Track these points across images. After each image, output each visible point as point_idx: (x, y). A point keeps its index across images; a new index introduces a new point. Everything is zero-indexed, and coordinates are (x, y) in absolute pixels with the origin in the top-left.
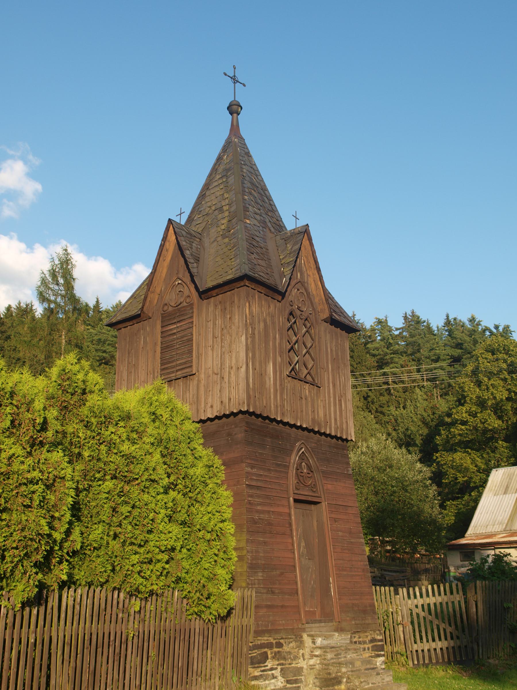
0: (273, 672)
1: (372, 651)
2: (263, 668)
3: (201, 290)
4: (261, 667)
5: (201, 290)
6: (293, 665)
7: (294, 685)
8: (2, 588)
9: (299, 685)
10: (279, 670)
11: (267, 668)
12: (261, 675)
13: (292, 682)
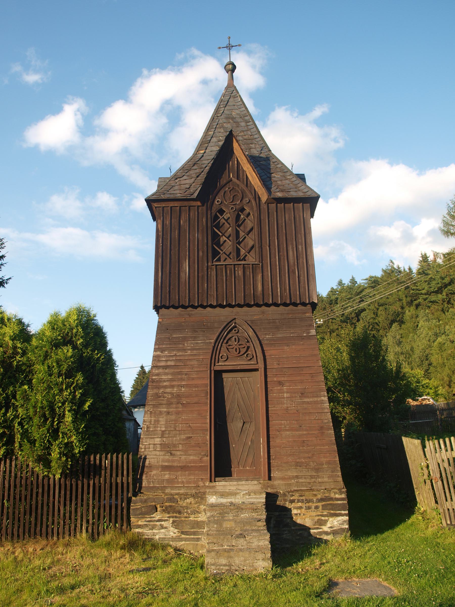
0: (162, 523)
1: (323, 509)
2: (149, 519)
3: (309, 204)
4: (147, 518)
5: (309, 204)
6: (191, 519)
7: (192, 537)
8: (454, 356)
9: (200, 536)
10: (171, 522)
11: (154, 519)
12: (146, 524)
13: (189, 533)
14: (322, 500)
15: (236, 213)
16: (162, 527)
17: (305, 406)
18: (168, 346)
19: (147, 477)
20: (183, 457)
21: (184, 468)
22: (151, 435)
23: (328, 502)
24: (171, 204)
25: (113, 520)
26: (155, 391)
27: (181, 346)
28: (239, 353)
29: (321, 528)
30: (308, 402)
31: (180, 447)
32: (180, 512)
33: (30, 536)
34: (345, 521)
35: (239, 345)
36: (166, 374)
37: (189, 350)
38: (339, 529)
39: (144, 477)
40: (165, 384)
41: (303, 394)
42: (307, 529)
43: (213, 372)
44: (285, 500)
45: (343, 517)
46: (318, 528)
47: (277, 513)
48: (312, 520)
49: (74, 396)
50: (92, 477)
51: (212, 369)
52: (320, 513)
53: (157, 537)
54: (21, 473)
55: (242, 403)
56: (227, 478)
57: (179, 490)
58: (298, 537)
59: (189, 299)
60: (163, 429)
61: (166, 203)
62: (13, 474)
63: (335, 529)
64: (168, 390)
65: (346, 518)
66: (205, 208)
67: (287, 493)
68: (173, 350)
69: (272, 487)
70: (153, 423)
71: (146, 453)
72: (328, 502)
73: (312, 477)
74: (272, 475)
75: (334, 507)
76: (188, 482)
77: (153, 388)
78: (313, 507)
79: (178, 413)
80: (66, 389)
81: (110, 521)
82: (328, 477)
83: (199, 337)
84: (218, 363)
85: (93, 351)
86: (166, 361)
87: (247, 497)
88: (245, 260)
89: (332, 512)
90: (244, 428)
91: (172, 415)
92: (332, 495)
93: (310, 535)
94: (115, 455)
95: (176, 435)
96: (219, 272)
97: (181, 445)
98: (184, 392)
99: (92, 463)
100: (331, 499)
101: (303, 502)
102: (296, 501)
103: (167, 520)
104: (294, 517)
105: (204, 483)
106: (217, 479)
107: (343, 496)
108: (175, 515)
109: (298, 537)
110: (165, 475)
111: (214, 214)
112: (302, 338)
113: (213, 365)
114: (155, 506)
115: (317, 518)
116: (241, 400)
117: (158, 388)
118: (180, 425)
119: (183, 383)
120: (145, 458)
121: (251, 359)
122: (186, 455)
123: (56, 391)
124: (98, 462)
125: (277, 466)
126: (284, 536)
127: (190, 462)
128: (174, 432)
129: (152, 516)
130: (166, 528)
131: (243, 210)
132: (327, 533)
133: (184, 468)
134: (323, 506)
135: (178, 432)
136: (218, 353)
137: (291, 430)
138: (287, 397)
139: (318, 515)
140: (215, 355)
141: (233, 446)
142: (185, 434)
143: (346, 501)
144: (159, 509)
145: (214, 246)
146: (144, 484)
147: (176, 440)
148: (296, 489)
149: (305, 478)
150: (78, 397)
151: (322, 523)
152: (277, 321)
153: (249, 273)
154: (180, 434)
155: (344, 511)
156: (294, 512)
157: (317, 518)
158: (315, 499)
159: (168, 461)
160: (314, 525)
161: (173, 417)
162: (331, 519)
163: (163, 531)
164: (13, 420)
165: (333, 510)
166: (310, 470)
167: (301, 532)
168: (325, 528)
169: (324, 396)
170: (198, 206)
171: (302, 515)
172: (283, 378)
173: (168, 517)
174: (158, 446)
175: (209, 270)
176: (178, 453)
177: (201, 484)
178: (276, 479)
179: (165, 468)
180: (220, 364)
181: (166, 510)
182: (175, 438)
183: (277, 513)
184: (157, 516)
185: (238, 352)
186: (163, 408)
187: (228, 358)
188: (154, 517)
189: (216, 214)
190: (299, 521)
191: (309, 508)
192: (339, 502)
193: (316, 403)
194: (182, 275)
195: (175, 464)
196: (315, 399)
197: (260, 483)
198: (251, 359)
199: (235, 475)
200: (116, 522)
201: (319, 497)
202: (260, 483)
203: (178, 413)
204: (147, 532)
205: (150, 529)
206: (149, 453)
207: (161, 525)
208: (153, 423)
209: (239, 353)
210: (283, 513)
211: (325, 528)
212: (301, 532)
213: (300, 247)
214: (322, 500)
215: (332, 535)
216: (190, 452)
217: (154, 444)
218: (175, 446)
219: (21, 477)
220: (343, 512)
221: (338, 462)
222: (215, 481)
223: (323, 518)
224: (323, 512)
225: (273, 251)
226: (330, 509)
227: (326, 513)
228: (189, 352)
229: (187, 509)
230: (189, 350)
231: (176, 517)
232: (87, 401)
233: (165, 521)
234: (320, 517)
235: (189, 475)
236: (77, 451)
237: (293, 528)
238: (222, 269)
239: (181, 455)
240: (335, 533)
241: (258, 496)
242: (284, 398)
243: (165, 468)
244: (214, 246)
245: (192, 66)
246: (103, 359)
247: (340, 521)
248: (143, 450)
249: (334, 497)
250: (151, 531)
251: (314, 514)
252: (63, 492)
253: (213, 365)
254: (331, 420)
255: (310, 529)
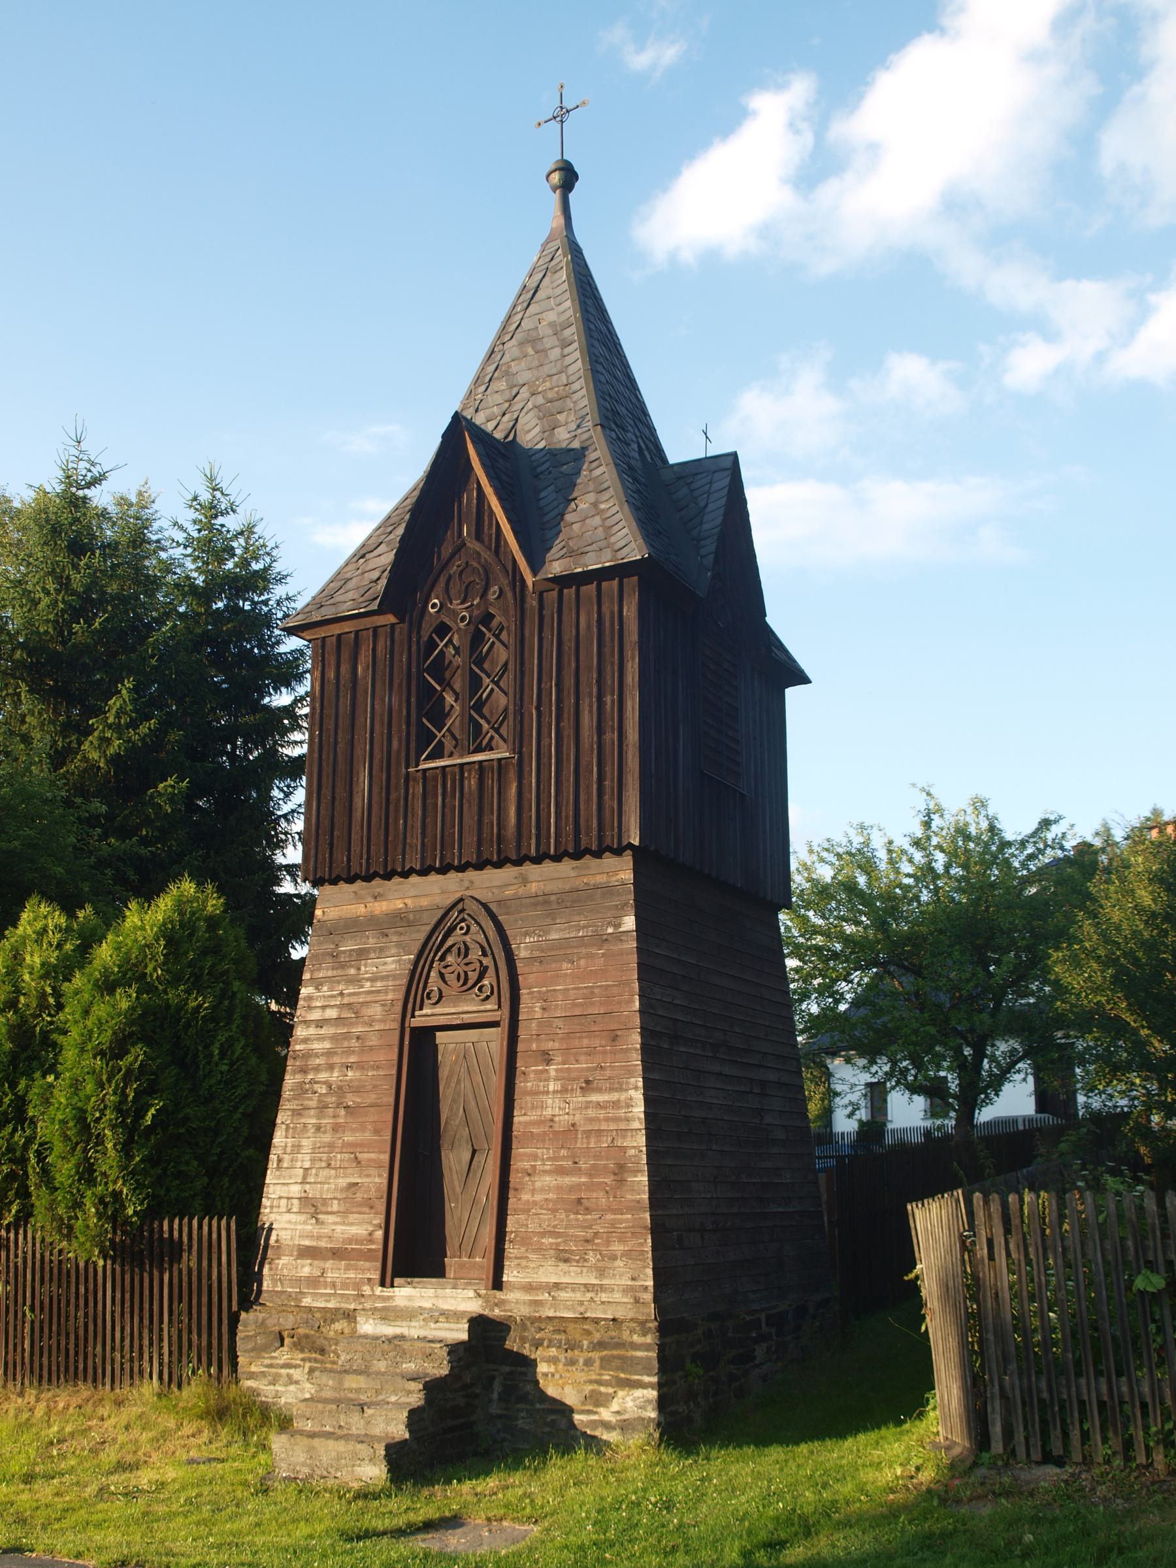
0: (292, 1371)
1: (602, 1367)
10: (307, 1370)
14: (601, 1345)
15: (472, 628)
16: (291, 1381)
17: (591, 1113)
18: (330, 973)
19: (271, 1269)
20: (339, 1228)
21: (336, 1254)
22: (284, 1178)
23: (615, 1352)
24: (336, 629)
25: (204, 1359)
26: (299, 1078)
27: (352, 971)
28: (465, 983)
29: (596, 1413)
30: (598, 1103)
31: (335, 1206)
32: (322, 1351)
33: (67, 1381)
34: (648, 1401)
35: (467, 964)
36: (321, 1038)
37: (367, 980)
38: (635, 1419)
39: (266, 1271)
40: (318, 1061)
41: (588, 1086)
42: (566, 1411)
43: (408, 1031)
44: (523, 1340)
45: (645, 1391)
46: (589, 1412)
47: (507, 1369)
48: (579, 1392)
49: (124, 1095)
50: (166, 1265)
51: (407, 1025)
52: (594, 1377)
53: (283, 1400)
54: (51, 1254)
55: (473, 1103)
56: (416, 1280)
57: (327, 1301)
58: (547, 1429)
59: (368, 859)
60: (307, 1165)
61: (324, 628)
62: (38, 1256)
63: (626, 1417)
64: (323, 1076)
65: (653, 1394)
66: (405, 626)
67: (528, 1323)
68: (339, 982)
69: (500, 1304)
70: (289, 1150)
71: (273, 1217)
72: (615, 1352)
73: (587, 1287)
74: (505, 1278)
75: (627, 1364)
76: (345, 1286)
77: (294, 1073)
78: (581, 1361)
79: (336, 1128)
80: (109, 1081)
81: (199, 1360)
82: (624, 1291)
83: (388, 947)
84: (421, 1009)
85: (188, 992)
86: (324, 1007)
87: (433, 1325)
88: (491, 749)
89: (622, 1375)
90: (474, 1162)
91: (325, 1132)
92: (625, 1335)
93: (572, 1425)
94: (177, 1221)
95: (330, 1178)
96: (429, 788)
97: (336, 1202)
98: (351, 1081)
99: (166, 1236)
100: (621, 1345)
101: (559, 1347)
102: (545, 1344)
103: (299, 1366)
104: (541, 1381)
105: (372, 1290)
106: (397, 1281)
107: (649, 1339)
108: (314, 1355)
109: (547, 1429)
110: (303, 1266)
111: (426, 639)
112: (603, 940)
113: (409, 1015)
114: (280, 1333)
115: (589, 1387)
116: (471, 1096)
117: (304, 1071)
118: (339, 1156)
119: (352, 1059)
120: (270, 1229)
121: (488, 998)
122: (343, 1224)
123: (90, 1087)
124: (176, 1234)
125: (516, 1258)
126: (520, 1422)
127: (350, 1241)
128: (326, 1172)
129: (273, 1354)
130: (297, 1382)
131: (487, 618)
132: (607, 1426)
133: (336, 1254)
134: (602, 1359)
135: (333, 1172)
136: (421, 986)
137: (560, 1171)
138: (554, 1092)
139: (591, 1382)
140: (415, 990)
141: (450, 1206)
142: (345, 1176)
143: (653, 1350)
144: (287, 1341)
145: (424, 720)
146: (265, 1287)
147: (328, 1190)
148: (551, 1315)
149: (573, 1290)
150: (131, 1098)
151: (599, 1400)
152: (553, 898)
153: (491, 783)
154: (336, 1177)
155: (648, 1375)
156: (542, 1368)
157: (589, 1387)
158: (585, 1343)
159: (311, 1237)
160: (583, 1404)
161: (327, 1138)
162: (621, 1393)
163: (292, 1388)
164: (26, 1147)
165: (623, 1371)
166: (585, 1270)
167: (554, 1417)
168: (606, 1414)
169: (636, 1088)
170: (393, 625)
171: (557, 1376)
172: (551, 1043)
173: (303, 1360)
174: (296, 1202)
175: (411, 783)
176: (330, 1219)
177: (367, 1290)
178: (513, 1287)
179: (307, 1253)
180: (424, 1012)
181: (298, 1346)
182: (326, 1186)
183: (507, 1369)
184: (283, 1355)
185: (461, 982)
186: (310, 1117)
187: (441, 997)
188: (275, 1358)
189: (431, 637)
190: (551, 1391)
191: (572, 1362)
192: (639, 1354)
193: (616, 1104)
194: (357, 801)
195: (323, 1244)
196: (615, 1096)
197: (479, 1296)
198: (488, 998)
199: (450, 1272)
200: (210, 1364)
201: (597, 1336)
202: (479, 1296)
203: (336, 1128)
204: (266, 1390)
205: (270, 1384)
206: (278, 1217)
207: (288, 1375)
208: (289, 1150)
209: (465, 983)
210: (520, 1369)
211: (606, 1414)
212: (554, 1417)
213: (608, 699)
214: (601, 1345)
215: (618, 1430)
216: (352, 1217)
217: (288, 1198)
218: (325, 1201)
219: (51, 1261)
220: (646, 1379)
221: (650, 1255)
222: (392, 1286)
223: (603, 1389)
224: (601, 1375)
225: (545, 720)
226: (618, 1369)
227: (607, 1377)
228: (368, 984)
229: (336, 1344)
230: (367, 980)
231: (316, 1360)
232: (152, 1105)
233: (296, 1367)
234: (595, 1387)
235: (347, 1269)
236: (130, 1211)
237: (538, 1406)
238: (435, 778)
239: (335, 1223)
240: (625, 1426)
241: (453, 1326)
242: (548, 1092)
243: (307, 1253)
244: (424, 720)
245: (888, 68)
246: (206, 1009)
247: (637, 1401)
248: (267, 1210)
249: (629, 1339)
250: (272, 1387)
251: (582, 1377)
252: (118, 1296)
253: (409, 1015)
254: (644, 1149)
255: (571, 1410)
